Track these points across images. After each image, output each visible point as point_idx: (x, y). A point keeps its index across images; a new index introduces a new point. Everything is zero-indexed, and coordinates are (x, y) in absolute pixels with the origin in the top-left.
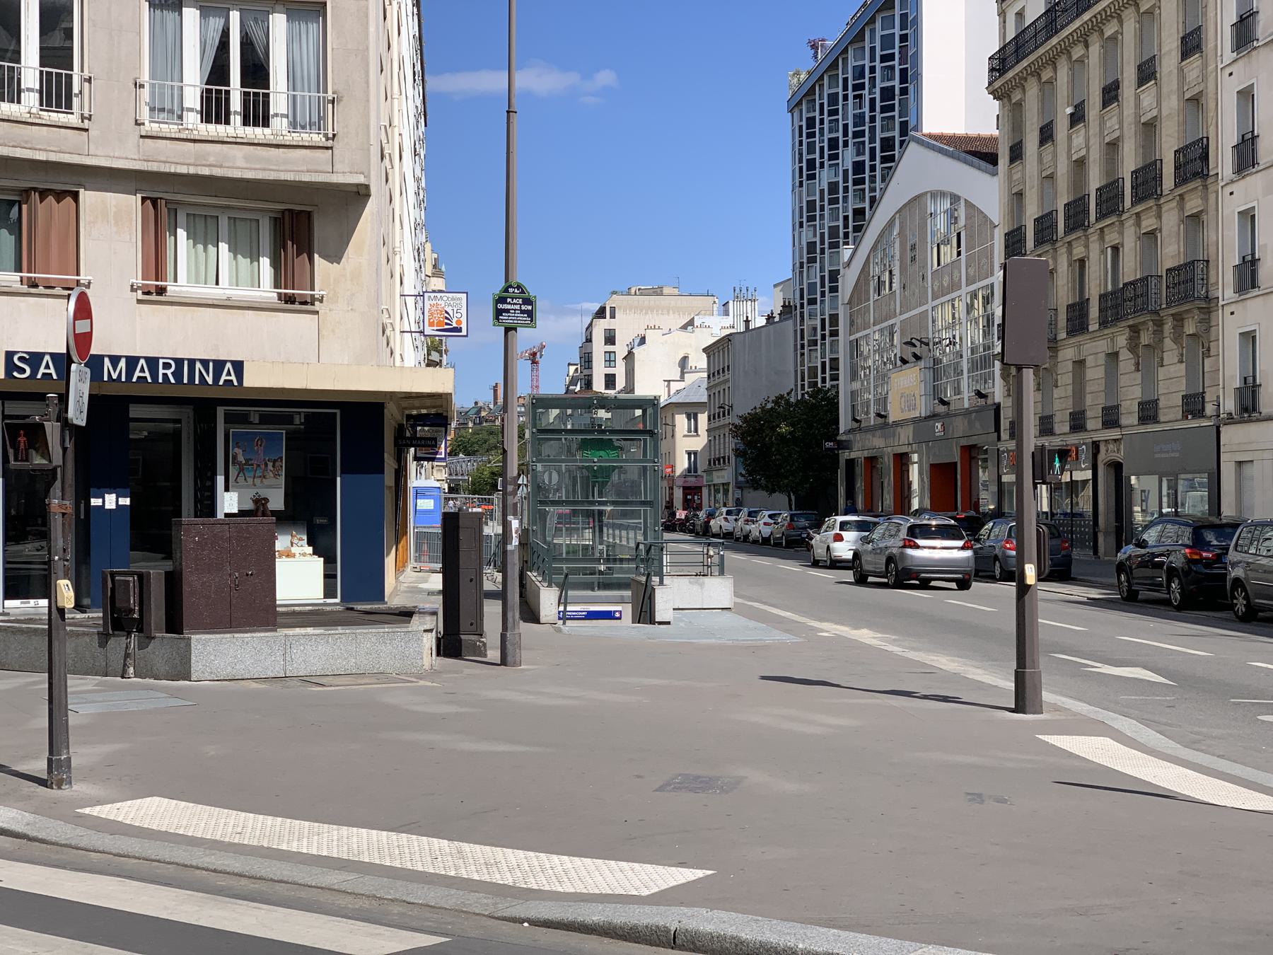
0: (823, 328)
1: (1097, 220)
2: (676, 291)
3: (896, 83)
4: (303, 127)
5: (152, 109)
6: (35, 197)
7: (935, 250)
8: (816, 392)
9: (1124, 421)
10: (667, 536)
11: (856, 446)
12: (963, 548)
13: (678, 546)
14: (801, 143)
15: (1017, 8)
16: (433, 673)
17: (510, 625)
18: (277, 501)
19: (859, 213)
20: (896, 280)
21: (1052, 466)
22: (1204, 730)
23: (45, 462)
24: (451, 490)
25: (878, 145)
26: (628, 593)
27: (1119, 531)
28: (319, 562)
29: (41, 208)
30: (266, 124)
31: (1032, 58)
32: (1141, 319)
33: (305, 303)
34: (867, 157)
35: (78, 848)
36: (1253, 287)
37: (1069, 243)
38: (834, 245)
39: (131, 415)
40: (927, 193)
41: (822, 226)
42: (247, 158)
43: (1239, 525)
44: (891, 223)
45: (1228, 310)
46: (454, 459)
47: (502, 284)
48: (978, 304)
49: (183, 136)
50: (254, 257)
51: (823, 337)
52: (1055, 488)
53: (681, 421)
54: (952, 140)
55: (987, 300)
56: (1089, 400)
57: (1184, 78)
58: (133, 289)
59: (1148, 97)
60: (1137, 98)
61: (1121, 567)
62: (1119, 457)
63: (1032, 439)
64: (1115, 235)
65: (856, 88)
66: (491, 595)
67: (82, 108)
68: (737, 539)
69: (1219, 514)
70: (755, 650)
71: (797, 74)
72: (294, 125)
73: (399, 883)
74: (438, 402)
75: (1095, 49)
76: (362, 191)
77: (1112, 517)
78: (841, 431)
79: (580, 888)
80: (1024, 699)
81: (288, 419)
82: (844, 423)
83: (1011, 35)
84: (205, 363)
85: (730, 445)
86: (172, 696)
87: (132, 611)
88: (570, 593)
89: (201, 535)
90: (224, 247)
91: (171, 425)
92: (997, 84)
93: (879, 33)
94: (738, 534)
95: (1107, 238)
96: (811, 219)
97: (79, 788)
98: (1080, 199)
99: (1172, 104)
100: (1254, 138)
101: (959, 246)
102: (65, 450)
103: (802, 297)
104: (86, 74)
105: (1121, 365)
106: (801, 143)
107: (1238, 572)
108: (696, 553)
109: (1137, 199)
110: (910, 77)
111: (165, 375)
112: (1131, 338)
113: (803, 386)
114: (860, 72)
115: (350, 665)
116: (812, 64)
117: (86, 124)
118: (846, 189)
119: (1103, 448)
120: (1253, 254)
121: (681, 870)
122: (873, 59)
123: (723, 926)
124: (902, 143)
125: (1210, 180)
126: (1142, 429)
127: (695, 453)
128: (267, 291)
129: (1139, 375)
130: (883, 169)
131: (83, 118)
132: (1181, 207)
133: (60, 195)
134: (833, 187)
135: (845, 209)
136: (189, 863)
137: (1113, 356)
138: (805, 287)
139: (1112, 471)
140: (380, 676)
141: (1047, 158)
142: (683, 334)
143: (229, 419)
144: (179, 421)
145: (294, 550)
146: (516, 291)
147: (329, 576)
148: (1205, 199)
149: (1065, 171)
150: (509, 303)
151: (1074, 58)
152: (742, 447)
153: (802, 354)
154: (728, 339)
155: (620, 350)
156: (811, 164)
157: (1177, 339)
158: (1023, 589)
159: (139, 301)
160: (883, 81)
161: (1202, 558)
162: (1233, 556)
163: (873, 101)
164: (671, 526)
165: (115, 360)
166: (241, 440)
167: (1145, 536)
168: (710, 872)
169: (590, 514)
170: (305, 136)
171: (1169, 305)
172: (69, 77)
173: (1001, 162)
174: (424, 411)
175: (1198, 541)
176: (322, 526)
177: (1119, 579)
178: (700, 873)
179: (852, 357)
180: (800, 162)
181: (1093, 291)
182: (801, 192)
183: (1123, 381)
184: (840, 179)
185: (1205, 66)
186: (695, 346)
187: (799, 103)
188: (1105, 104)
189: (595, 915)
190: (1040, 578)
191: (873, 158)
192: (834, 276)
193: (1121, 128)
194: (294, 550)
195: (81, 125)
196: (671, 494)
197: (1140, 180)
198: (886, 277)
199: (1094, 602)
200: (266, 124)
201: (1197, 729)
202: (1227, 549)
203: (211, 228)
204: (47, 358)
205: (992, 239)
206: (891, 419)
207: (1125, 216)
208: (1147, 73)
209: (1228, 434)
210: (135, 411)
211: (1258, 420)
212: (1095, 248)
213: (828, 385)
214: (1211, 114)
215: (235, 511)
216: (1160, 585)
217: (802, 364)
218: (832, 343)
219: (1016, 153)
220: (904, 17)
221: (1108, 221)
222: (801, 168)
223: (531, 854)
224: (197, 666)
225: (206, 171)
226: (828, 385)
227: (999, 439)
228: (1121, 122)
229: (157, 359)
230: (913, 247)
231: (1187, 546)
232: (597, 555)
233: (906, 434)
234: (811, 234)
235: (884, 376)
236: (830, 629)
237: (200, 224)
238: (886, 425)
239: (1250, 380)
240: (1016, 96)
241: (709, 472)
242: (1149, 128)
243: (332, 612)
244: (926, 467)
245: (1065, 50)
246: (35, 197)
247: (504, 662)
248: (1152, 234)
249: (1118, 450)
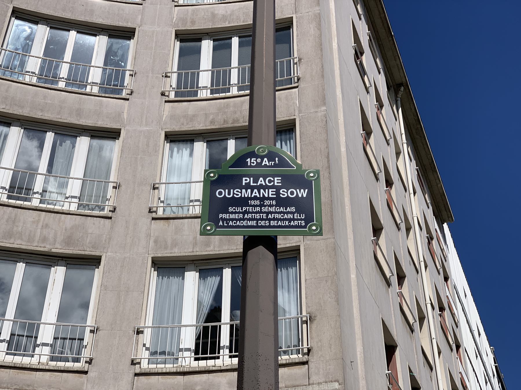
146: (266, 161)
150: (248, 186)
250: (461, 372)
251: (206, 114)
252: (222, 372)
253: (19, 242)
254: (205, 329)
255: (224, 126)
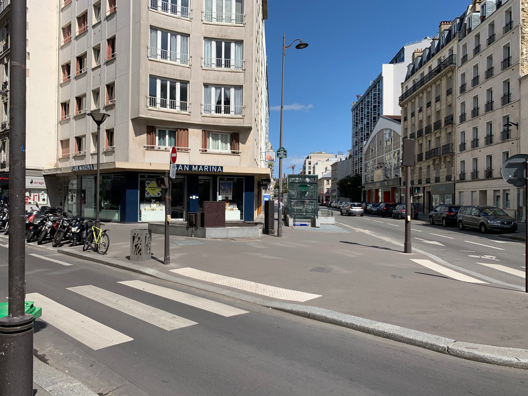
0: (359, 161)
1: (425, 134)
2: (325, 153)
3: (377, 104)
4: (237, 114)
5: (204, 110)
6: (179, 130)
7: (386, 142)
8: (357, 175)
9: (431, 182)
10: (320, 207)
11: (366, 187)
12: (361, 209)
13: (323, 209)
14: (354, 118)
15: (406, 85)
16: (261, 238)
17: (280, 227)
18: (230, 198)
19: (368, 134)
20: (376, 149)
21: (415, 191)
22: (454, 259)
23: (164, 187)
24: (274, 196)
25: (372, 118)
26: (310, 220)
27: (429, 208)
28: (239, 212)
29: (180, 132)
30: (229, 113)
31: (409, 97)
32: (436, 158)
33: (237, 153)
34: (370, 121)
35: (166, 280)
36: (464, 150)
37: (418, 140)
38: (362, 142)
39: (199, 178)
40: (383, 129)
41: (359, 137)
42: (225, 121)
43: (460, 207)
44: (375, 136)
45: (458, 155)
46: (275, 189)
47: (279, 147)
48: (396, 155)
49: (211, 116)
50: (226, 143)
51: (359, 162)
52: (414, 198)
53: (325, 181)
54: (390, 117)
55: (398, 154)
56: (423, 177)
57: (447, 100)
58: (200, 151)
59: (438, 105)
60: (435, 105)
61: (431, 216)
62: (430, 190)
63: (409, 185)
64: (429, 138)
65: (367, 105)
66: (276, 219)
67: (189, 110)
68: (338, 208)
69: (455, 204)
70: (339, 234)
71: (354, 103)
72: (235, 113)
73: (241, 294)
74: (267, 176)
75: (425, 94)
76: (250, 128)
77: (428, 205)
78: (363, 184)
79: (286, 299)
80: (407, 249)
81: (233, 179)
82: (363, 182)
83: (404, 92)
84: (215, 167)
85: (336, 186)
86: (201, 242)
87: (193, 222)
88: (296, 219)
89: (209, 205)
90: (220, 141)
91: (208, 181)
92: (401, 103)
93: (373, 93)
94: (338, 207)
95: (427, 139)
96: (356, 135)
97: (171, 265)
98: (421, 130)
99: (444, 107)
100: (465, 114)
101: (391, 141)
102: (169, 184)
103: (354, 154)
104: (190, 103)
105: (431, 168)
106: (354, 118)
107: (460, 218)
108: (326, 211)
109: (435, 129)
110: (380, 102)
111: (206, 170)
112: (433, 162)
113: (354, 174)
114: (368, 102)
115: (242, 235)
116: (357, 101)
117: (190, 114)
118: (365, 129)
119: (426, 188)
120: (464, 142)
121: (313, 294)
122: (371, 99)
123: (322, 313)
124: (378, 118)
125: (454, 125)
126: (436, 184)
127: (328, 189)
128: (229, 151)
129: (435, 171)
130: (374, 112)
131: (189, 112)
132: (446, 131)
133: (184, 130)
134: (362, 128)
135: (364, 133)
136: (191, 285)
137: (429, 167)
138: (355, 151)
139: (428, 193)
140: (249, 238)
141: (413, 120)
142: (326, 162)
143: (220, 179)
144: (209, 180)
145: (234, 209)
147: (241, 215)
148: (452, 129)
149: (417, 123)
151: (420, 97)
152: (339, 187)
153: (354, 167)
154: (336, 163)
155: (312, 166)
156: (357, 123)
157: (445, 162)
158: (407, 222)
159: (201, 153)
160: (374, 104)
161: (451, 215)
162: (459, 214)
163: (371, 108)
164: (322, 205)
165: (195, 166)
166: (224, 184)
167: (437, 209)
168: (321, 296)
169: (301, 202)
170: (238, 116)
171: (443, 154)
172: (186, 103)
173: (402, 121)
174: (265, 178)
175: (450, 211)
176: (240, 203)
177: (430, 219)
178: (318, 296)
179: (365, 167)
180: (354, 122)
181: (424, 151)
182: (354, 130)
183: (431, 172)
184: (363, 126)
185: (453, 97)
186: (329, 165)
187: (354, 109)
188: (427, 107)
189: (288, 307)
190: (411, 219)
191: (371, 121)
192: (361, 149)
193: (431, 113)
194: (234, 209)
195: (189, 114)
196: (323, 198)
197: (436, 125)
198: (374, 149)
199: (424, 225)
200: (229, 113)
201: (452, 258)
202: (457, 213)
203: (217, 138)
204: (180, 165)
205: (400, 139)
206: (374, 181)
207: (432, 133)
208: (438, 99)
209: (457, 185)
210: (200, 177)
211: (465, 182)
212: (424, 141)
213: (360, 173)
214: (454, 109)
215: (221, 200)
216: (440, 221)
217: (354, 169)
218: (361, 164)
219: (406, 119)
220: (379, 89)
221: (428, 135)
222: (354, 124)
223: (275, 287)
224: (207, 235)
225: (216, 124)
226: (360, 173)
227: (401, 186)
228: (431, 111)
229: (204, 166)
230: (380, 141)
231: (447, 212)
232: (303, 211)
233: (378, 185)
234: (356, 139)
235: (373, 171)
236: (358, 230)
237: (215, 136)
238: (373, 183)
239: (463, 172)
240: (406, 106)
241: (331, 193)
242: (438, 113)
243: (240, 223)
244: (383, 192)
245: (418, 95)
246: (179, 130)
247: (278, 236)
248: (439, 138)
249: (430, 189)
251: (216, 31)
253: (168, 75)
254: (217, 106)
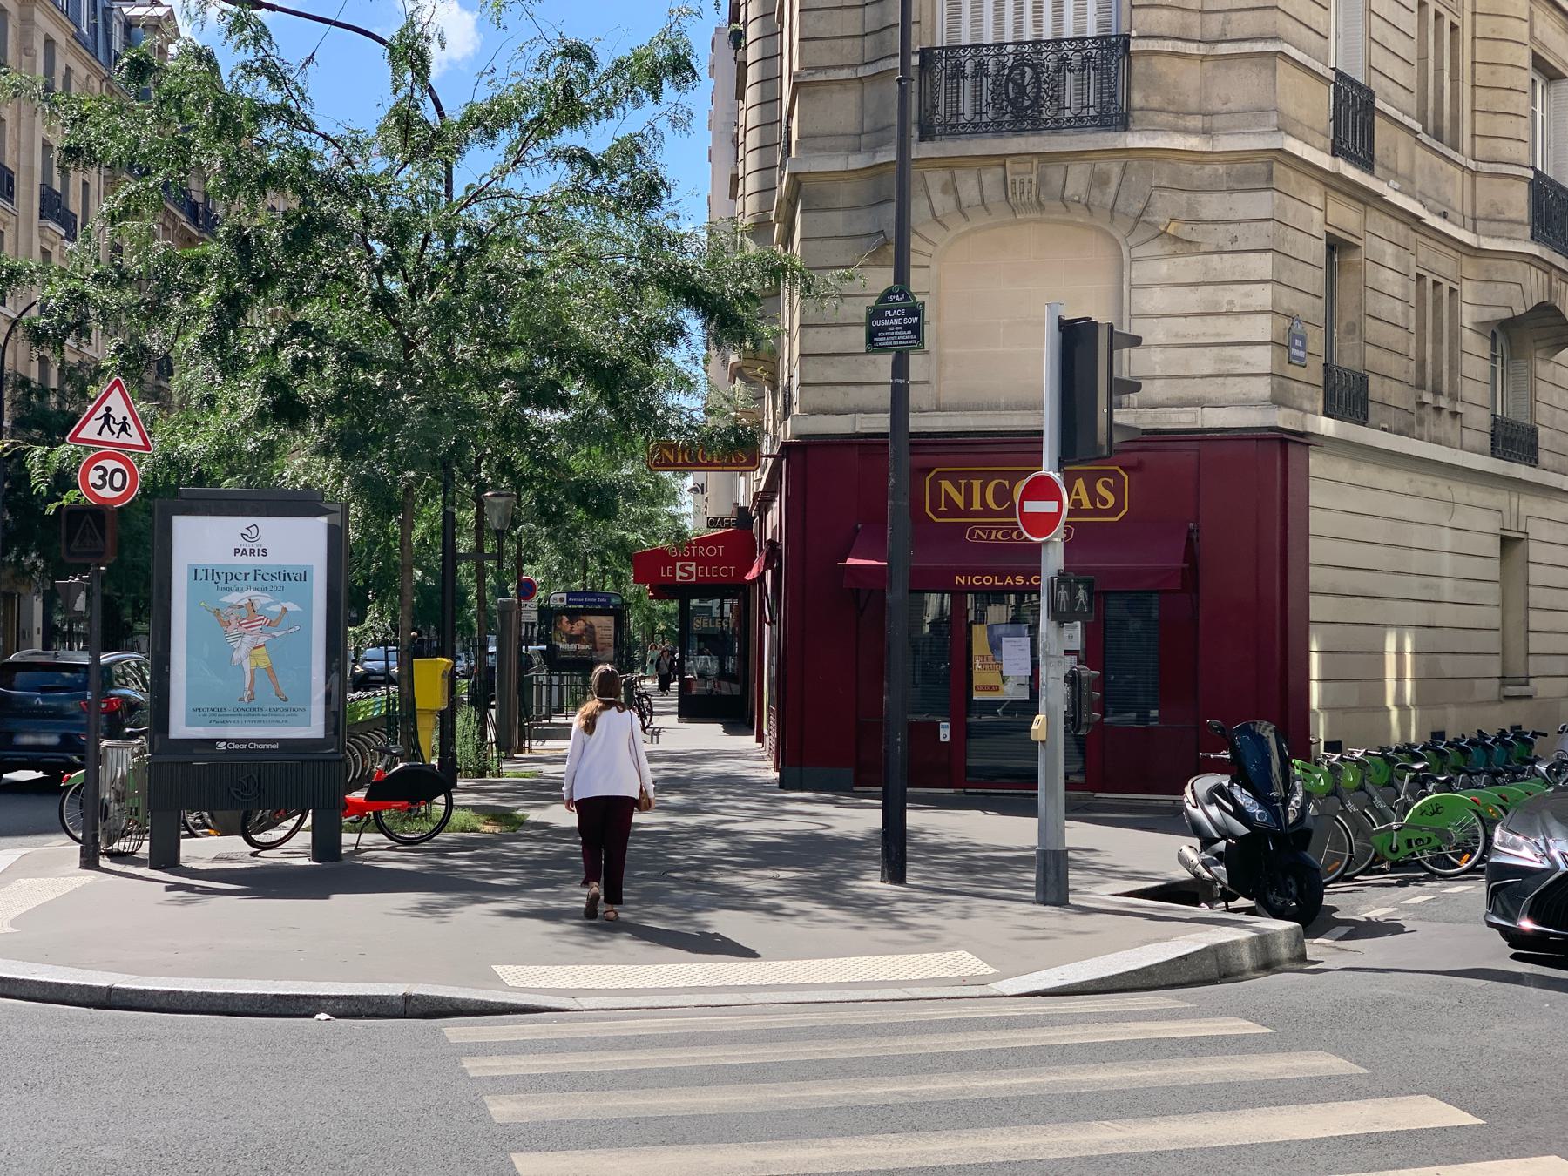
150: (888, 317)
250: (1534, 732)
252: (401, 1003)
255: (1110, 1030)
